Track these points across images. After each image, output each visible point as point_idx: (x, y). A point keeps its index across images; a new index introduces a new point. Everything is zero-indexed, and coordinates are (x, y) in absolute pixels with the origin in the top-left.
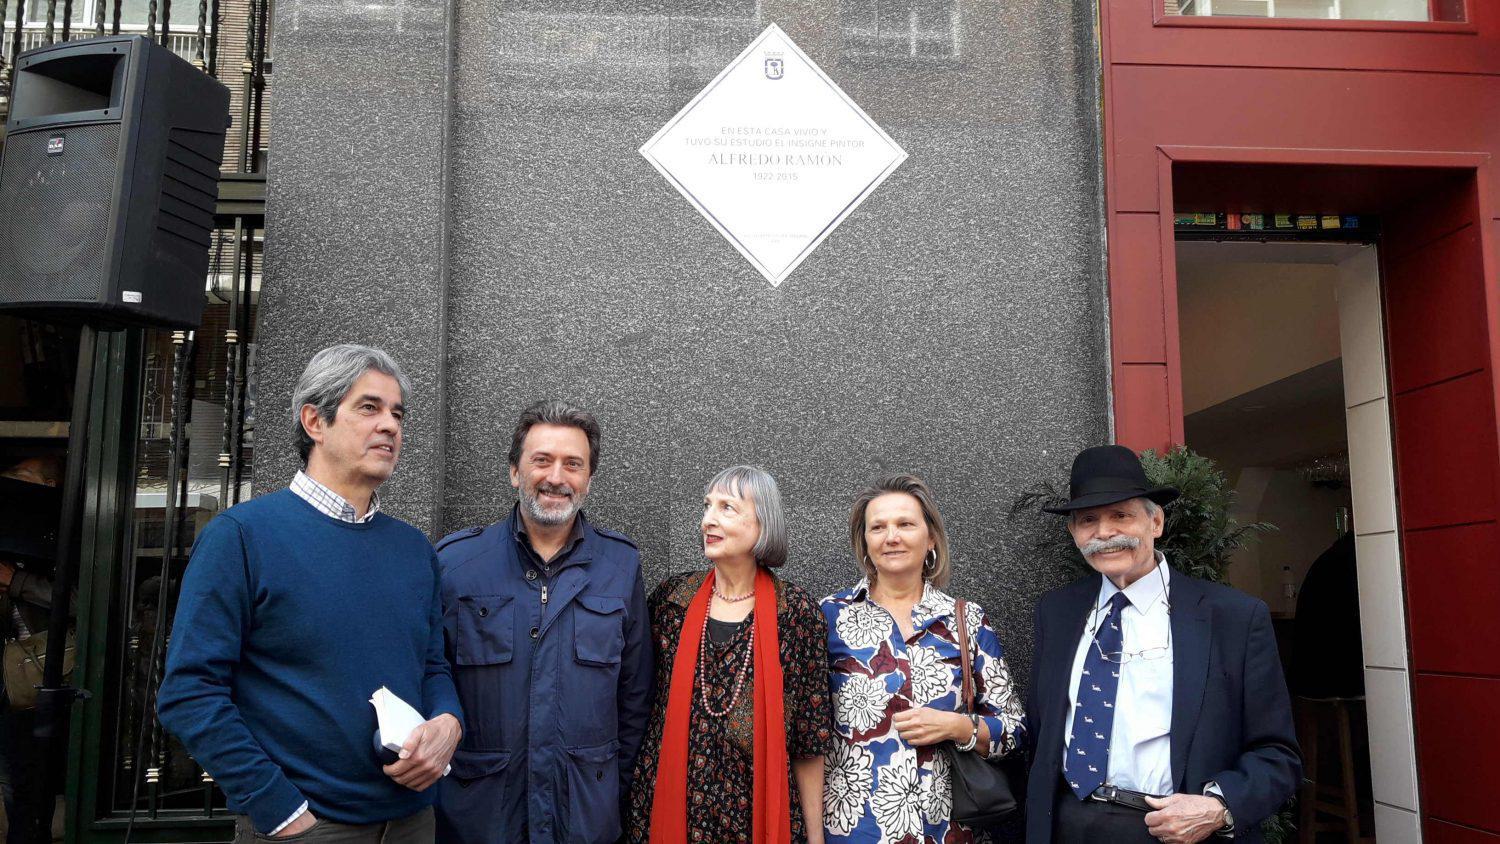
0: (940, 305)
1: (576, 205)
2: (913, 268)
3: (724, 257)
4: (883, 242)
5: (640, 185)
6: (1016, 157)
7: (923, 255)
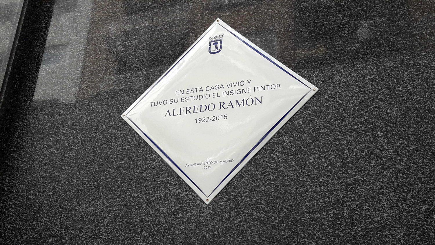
0: (353, 211)
1: (75, 159)
2: (325, 179)
3: (170, 184)
4: (298, 159)
5: (118, 139)
6: (418, 75)
7: (334, 167)
